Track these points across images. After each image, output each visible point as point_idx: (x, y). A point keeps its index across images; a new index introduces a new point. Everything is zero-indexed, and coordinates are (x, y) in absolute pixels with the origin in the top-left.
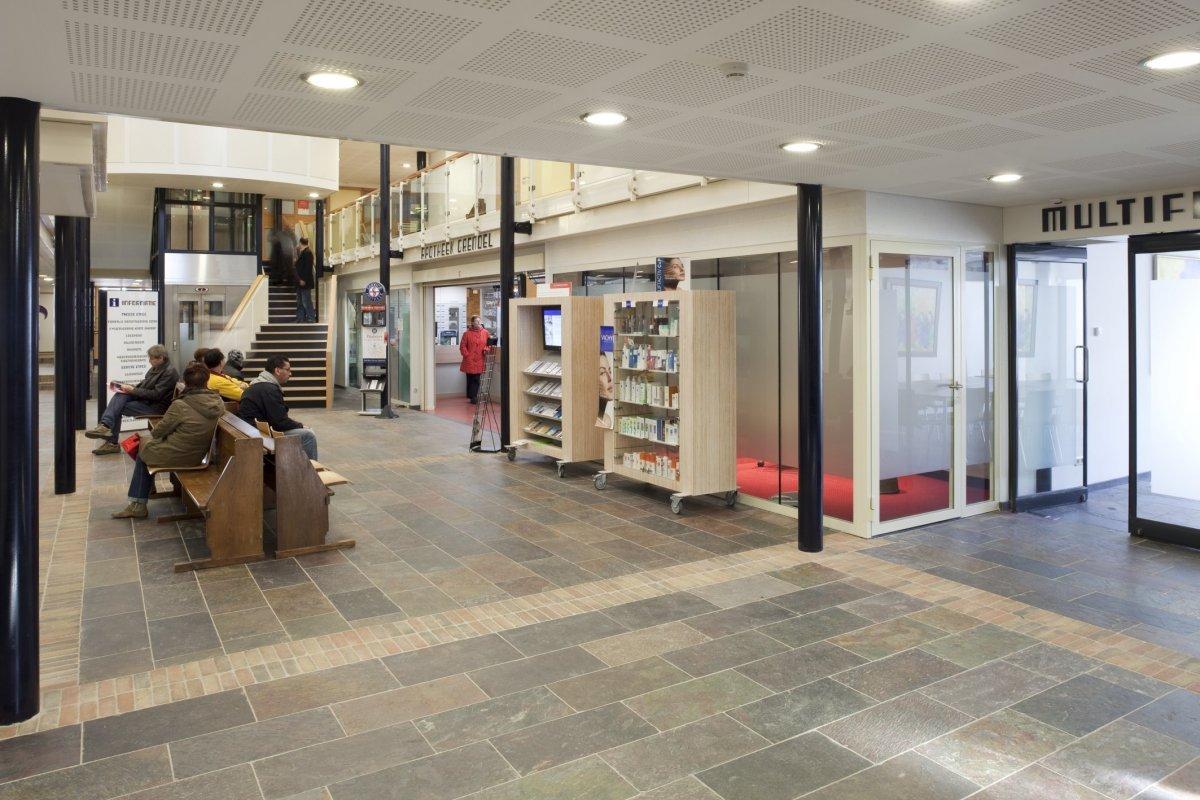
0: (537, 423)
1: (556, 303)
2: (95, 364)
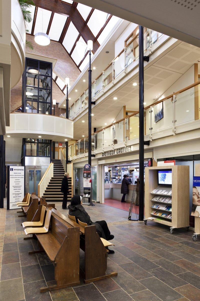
0: (155, 212)
1: (169, 168)
2: (6, 188)
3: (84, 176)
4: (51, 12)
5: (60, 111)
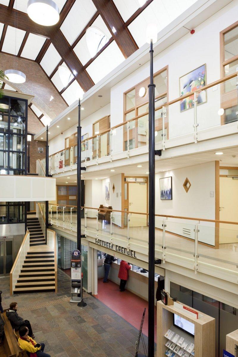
3: (72, 266)
4: (25, 32)
5: (36, 144)
